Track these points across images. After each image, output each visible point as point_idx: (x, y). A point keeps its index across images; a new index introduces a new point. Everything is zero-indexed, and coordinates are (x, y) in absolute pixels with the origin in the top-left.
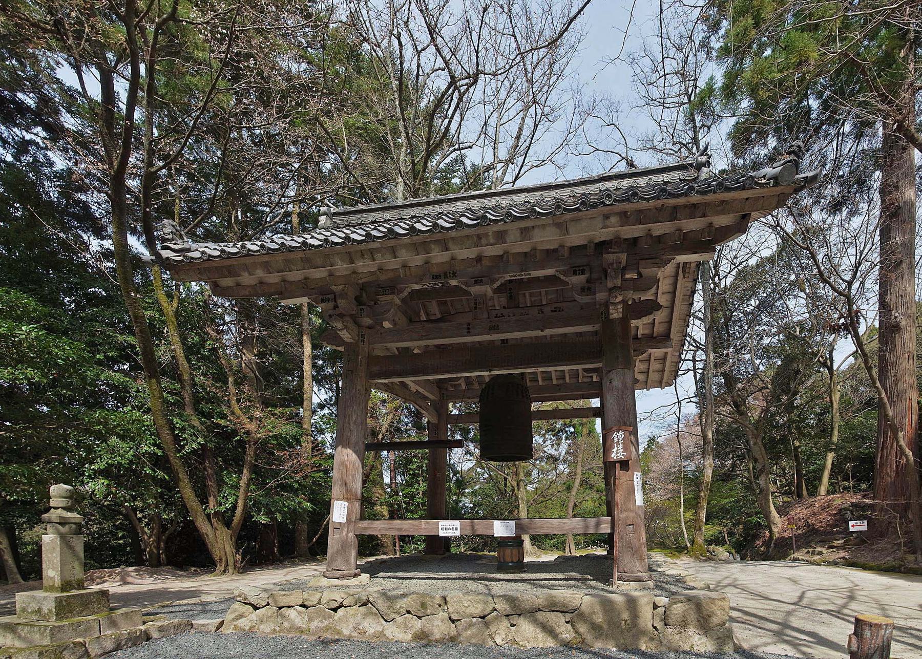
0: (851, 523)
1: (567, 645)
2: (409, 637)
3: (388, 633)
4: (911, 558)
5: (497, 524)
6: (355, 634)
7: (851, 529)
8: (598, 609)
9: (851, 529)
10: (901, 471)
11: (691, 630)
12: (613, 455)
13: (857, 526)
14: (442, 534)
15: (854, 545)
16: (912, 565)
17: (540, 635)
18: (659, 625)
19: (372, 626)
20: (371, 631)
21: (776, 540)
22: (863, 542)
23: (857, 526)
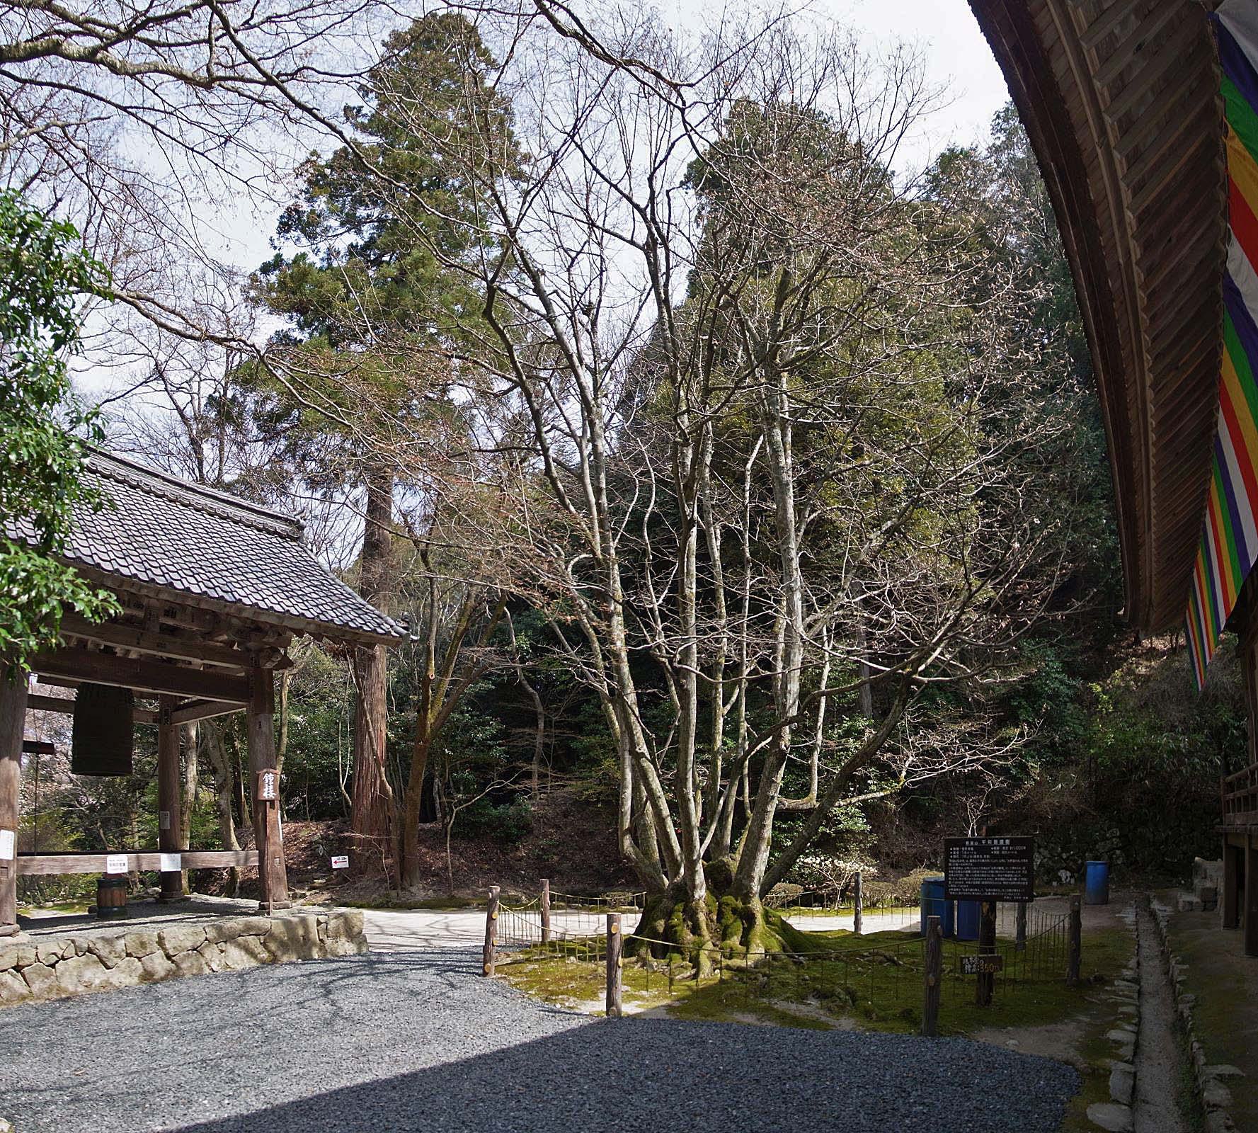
0: (334, 859)
1: (263, 962)
2: (136, 980)
3: (115, 981)
4: (393, 893)
5: (164, 857)
6: (81, 989)
7: (334, 866)
8: (282, 929)
9: (334, 866)
10: (380, 801)
11: (343, 939)
12: (265, 794)
13: (340, 862)
14: (110, 871)
15: (337, 884)
16: (395, 901)
17: (246, 957)
18: (323, 937)
19: (96, 975)
20: (97, 982)
21: (242, 883)
22: (345, 880)
23: (340, 862)
